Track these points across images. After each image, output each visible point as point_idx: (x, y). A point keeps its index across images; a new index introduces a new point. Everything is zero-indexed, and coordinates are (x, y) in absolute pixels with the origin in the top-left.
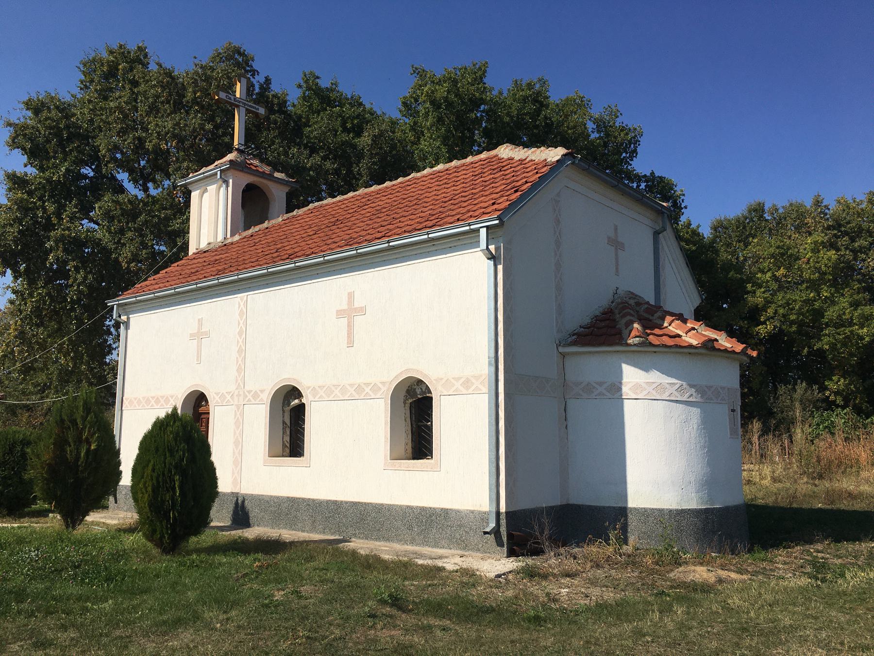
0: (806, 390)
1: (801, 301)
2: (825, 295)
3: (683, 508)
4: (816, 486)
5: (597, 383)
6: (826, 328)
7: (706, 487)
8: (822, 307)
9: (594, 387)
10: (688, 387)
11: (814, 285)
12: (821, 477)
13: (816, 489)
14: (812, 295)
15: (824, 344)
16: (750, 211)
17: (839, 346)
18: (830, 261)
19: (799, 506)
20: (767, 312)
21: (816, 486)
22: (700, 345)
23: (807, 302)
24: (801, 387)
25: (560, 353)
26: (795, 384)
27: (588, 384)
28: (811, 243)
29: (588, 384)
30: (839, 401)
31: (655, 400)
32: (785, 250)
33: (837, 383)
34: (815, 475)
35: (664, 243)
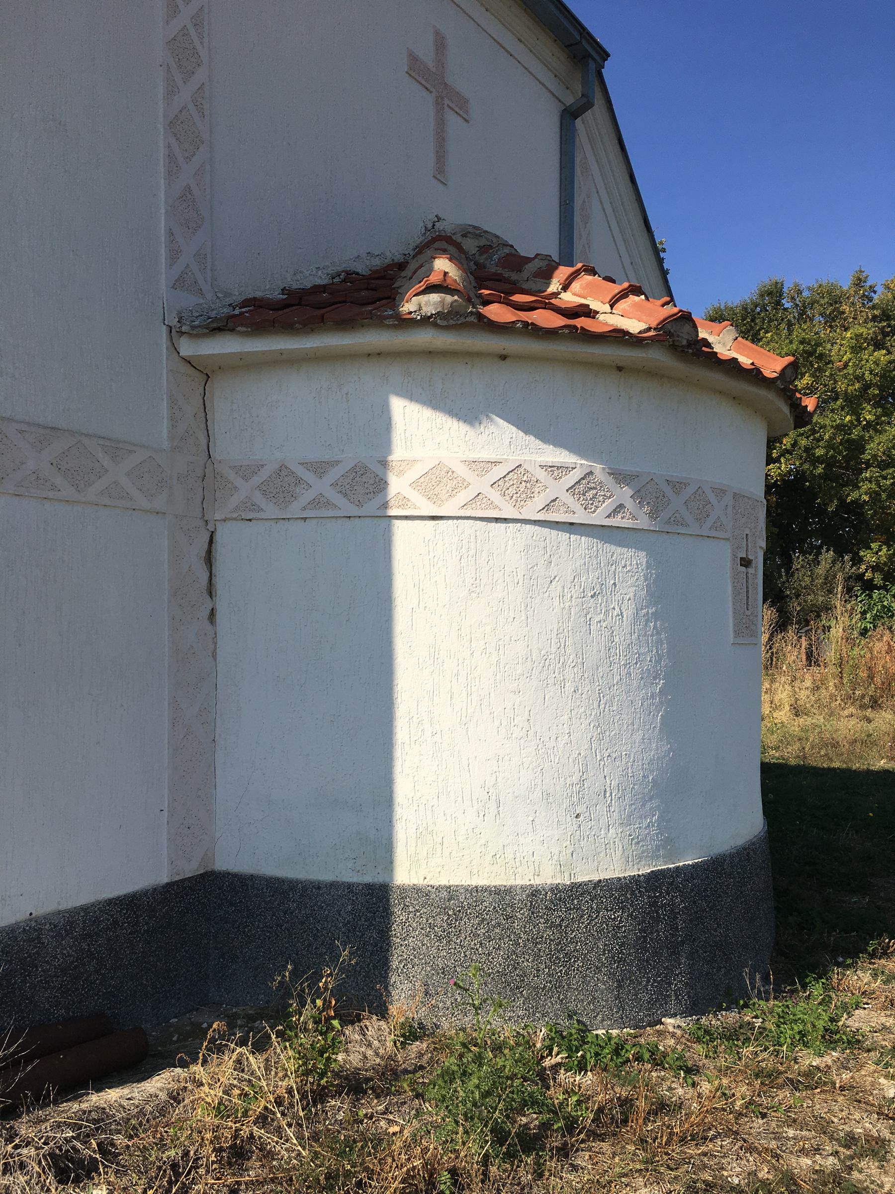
0: (834, 562)
1: (832, 427)
2: (867, 418)
3: (580, 879)
4: (869, 721)
5: (305, 465)
6: (866, 469)
7: (655, 803)
8: (862, 437)
9: (299, 481)
10: (609, 481)
11: (853, 404)
12: (875, 704)
13: (871, 727)
14: (848, 418)
15: (862, 493)
16: (762, 295)
17: (884, 496)
18: (878, 365)
19: (844, 766)
20: (781, 443)
21: (869, 721)
22: (652, 333)
23: (840, 428)
24: (828, 556)
25: (187, 361)
26: (819, 553)
27: (282, 469)
28: (851, 338)
29: (282, 469)
30: (878, 579)
31: (497, 520)
32: (812, 346)
33: (877, 553)
34: (866, 700)
35: (587, 147)
